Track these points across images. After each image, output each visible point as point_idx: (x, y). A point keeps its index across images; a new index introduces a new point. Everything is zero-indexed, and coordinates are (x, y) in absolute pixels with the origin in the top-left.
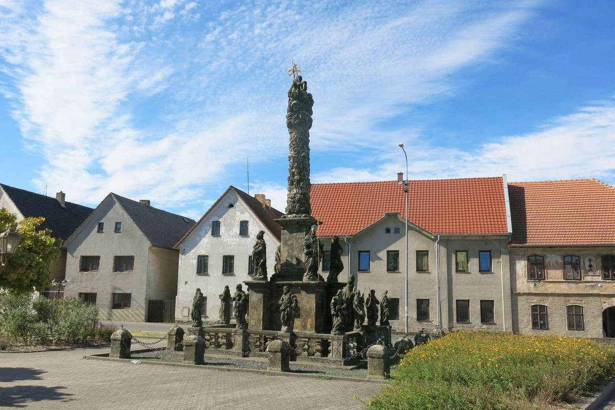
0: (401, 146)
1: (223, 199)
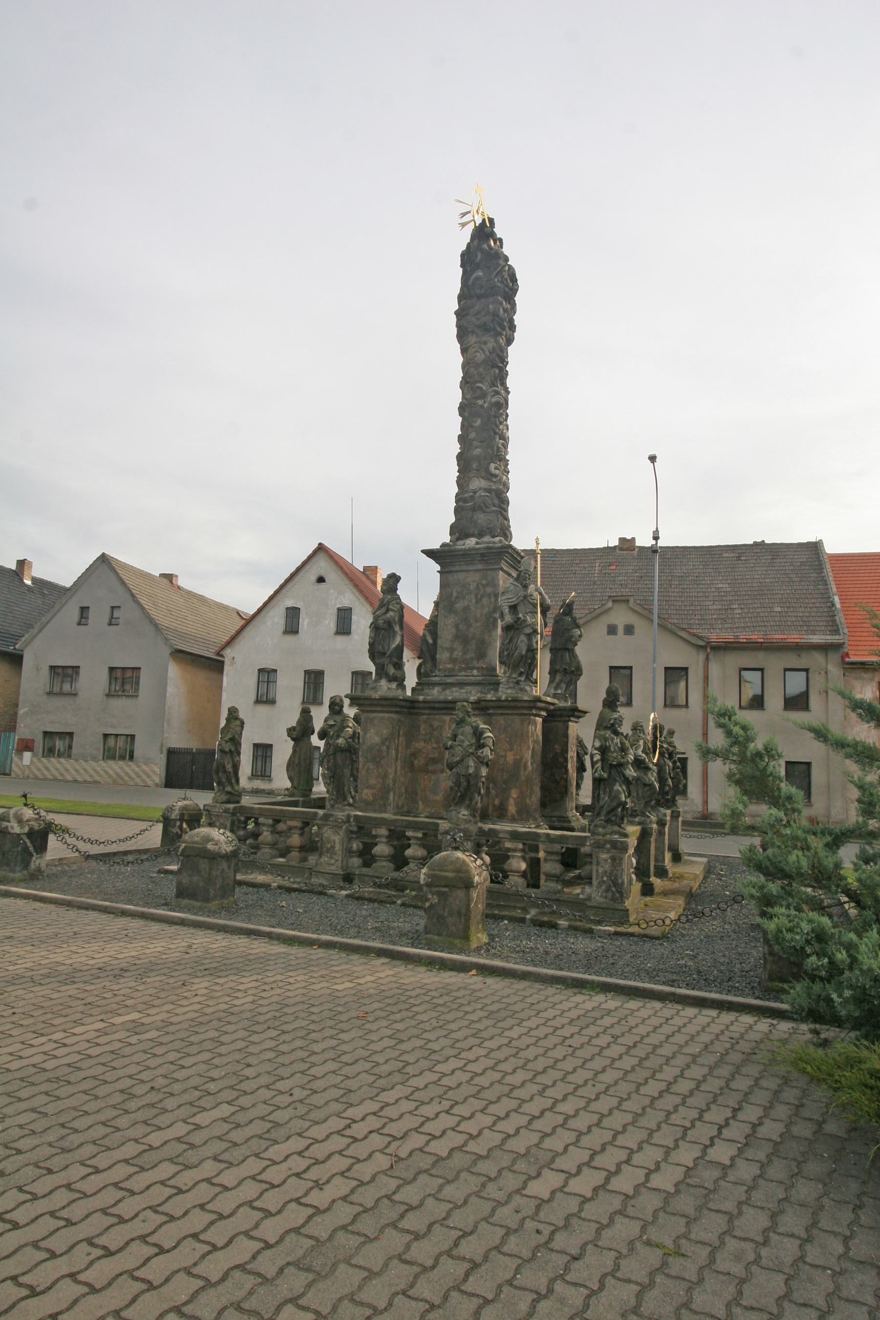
0: (653, 459)
1: (307, 567)
